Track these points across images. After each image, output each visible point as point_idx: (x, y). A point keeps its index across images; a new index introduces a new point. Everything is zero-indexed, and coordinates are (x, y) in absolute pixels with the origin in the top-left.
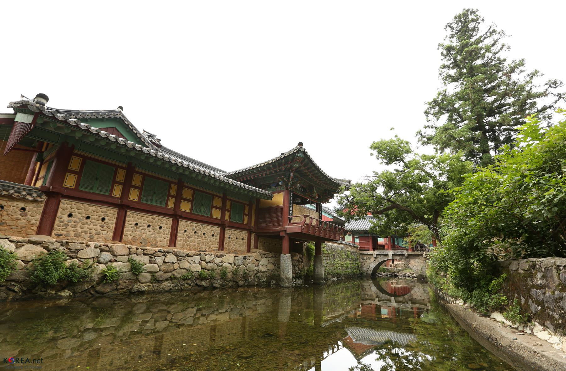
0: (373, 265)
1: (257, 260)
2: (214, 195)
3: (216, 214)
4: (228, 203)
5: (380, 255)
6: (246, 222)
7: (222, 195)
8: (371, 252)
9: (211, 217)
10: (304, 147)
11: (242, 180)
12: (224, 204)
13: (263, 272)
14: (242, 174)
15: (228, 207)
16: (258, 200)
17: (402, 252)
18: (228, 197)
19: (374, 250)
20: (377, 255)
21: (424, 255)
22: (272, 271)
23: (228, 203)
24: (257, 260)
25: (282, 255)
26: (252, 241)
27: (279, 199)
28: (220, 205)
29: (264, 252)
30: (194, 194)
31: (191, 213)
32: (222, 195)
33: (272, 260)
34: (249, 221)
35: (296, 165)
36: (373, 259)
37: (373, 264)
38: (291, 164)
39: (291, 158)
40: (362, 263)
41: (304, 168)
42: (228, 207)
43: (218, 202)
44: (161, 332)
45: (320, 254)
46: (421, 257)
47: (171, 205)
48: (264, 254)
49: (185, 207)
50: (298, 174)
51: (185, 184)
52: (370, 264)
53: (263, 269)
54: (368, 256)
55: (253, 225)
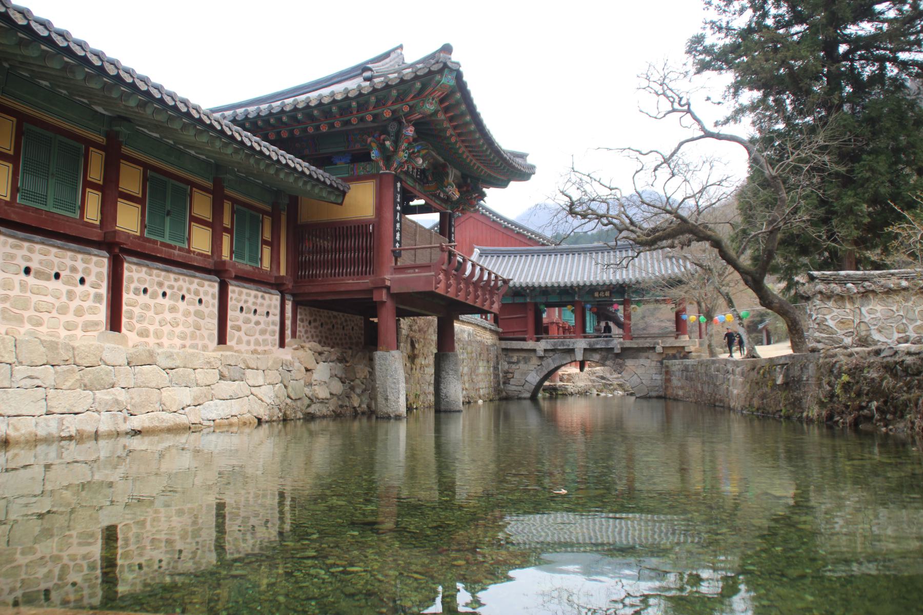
0: (533, 378)
1: (307, 370)
2: (193, 185)
3: (201, 241)
4: (227, 207)
5: (554, 350)
6: (266, 264)
7: (209, 184)
8: (530, 344)
9: (189, 251)
10: (454, 57)
11: (272, 137)
12: (217, 210)
13: (323, 401)
14: (279, 120)
15: (227, 222)
16: (294, 202)
17: (607, 342)
18: (228, 192)
19: (538, 340)
20: (546, 351)
21: (659, 349)
22: (339, 397)
23: (227, 207)
24: (307, 370)
25: (378, 354)
26: (288, 323)
27: (362, 200)
28: (207, 215)
29: (319, 348)
30: (145, 179)
31: (142, 237)
32: (209, 184)
33: (338, 368)
34: (275, 259)
35: (430, 107)
36: (535, 361)
37: (534, 374)
38: (411, 103)
39: (418, 85)
40: (507, 372)
41: (443, 117)
42: (227, 222)
43: (202, 207)
44: (852, 346)
45: (452, 349)
46: (650, 354)
47: (93, 214)
48: (320, 354)
49: (128, 220)
50: (417, 130)
51: (125, 150)
52: (525, 374)
53: (323, 393)
54: (523, 355)
55: (283, 272)
